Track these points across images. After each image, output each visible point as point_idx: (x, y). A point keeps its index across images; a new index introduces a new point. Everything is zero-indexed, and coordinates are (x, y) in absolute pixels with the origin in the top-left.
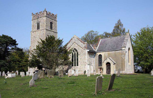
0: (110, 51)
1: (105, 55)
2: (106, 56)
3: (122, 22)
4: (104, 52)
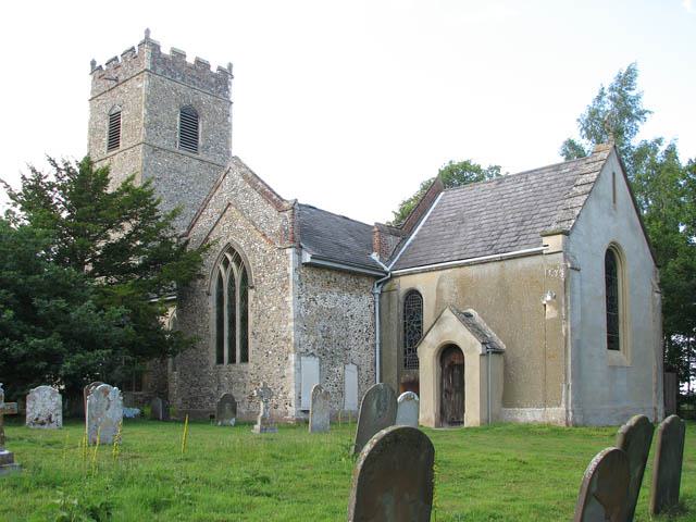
0: (468, 264)
1: (439, 291)
2: (446, 298)
3: (646, 92)
4: (437, 269)
